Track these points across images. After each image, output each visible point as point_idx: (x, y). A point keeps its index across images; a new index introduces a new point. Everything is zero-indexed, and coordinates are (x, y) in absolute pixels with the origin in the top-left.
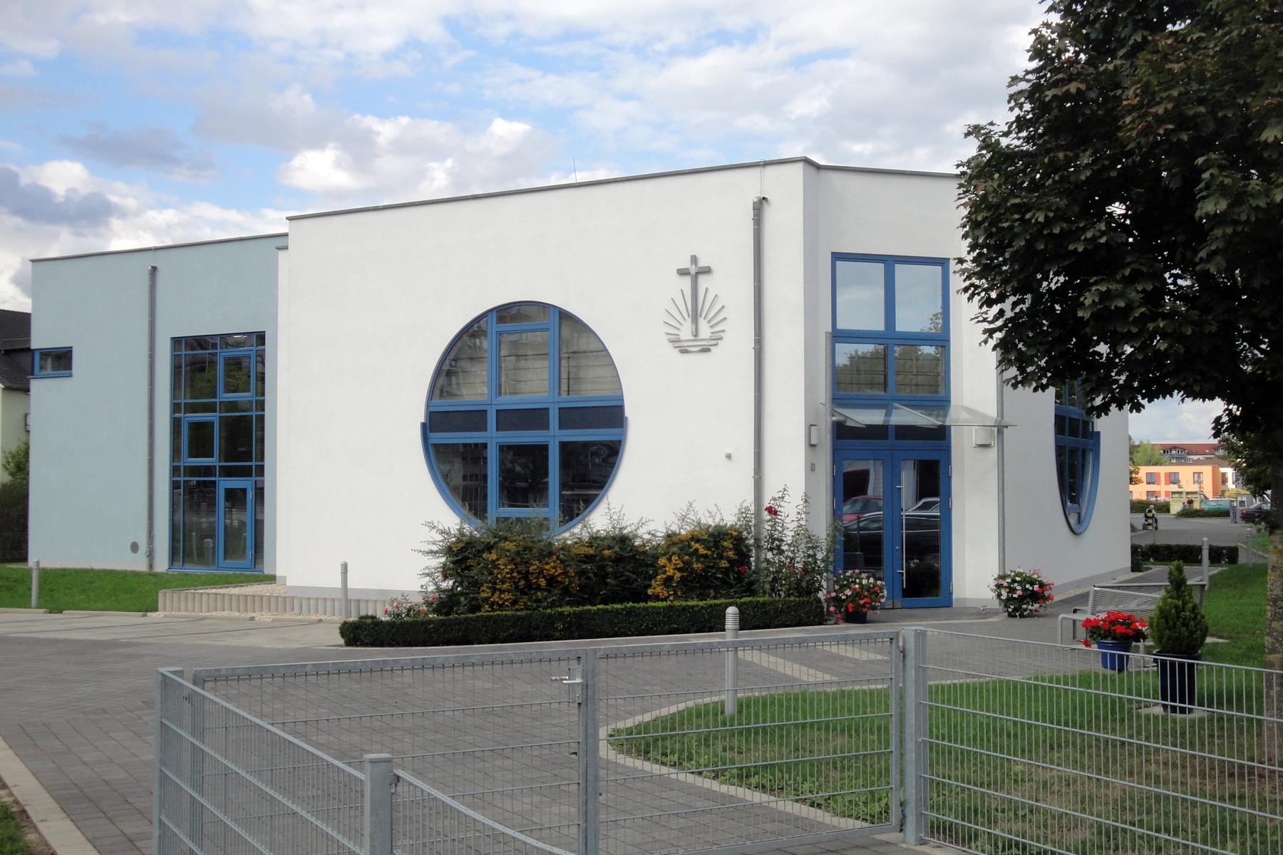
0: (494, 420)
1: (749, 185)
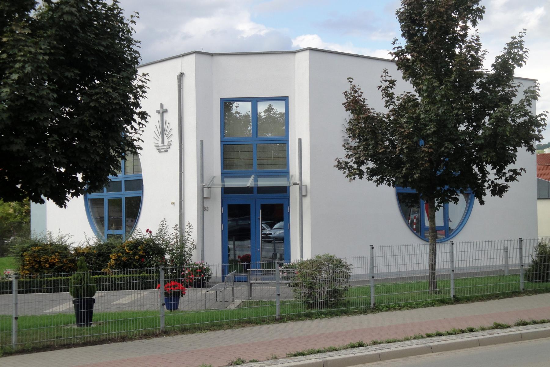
0: (124, 187)
1: (176, 66)
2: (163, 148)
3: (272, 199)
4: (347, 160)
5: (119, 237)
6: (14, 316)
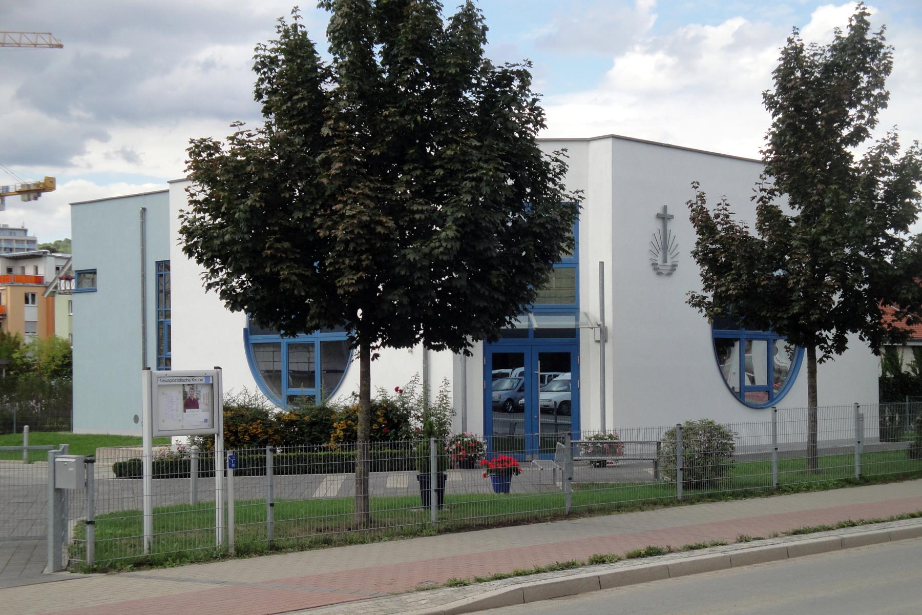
2: (665, 269)
3: (554, 346)
4: (704, 294)
5: (311, 398)
6: (269, 502)
